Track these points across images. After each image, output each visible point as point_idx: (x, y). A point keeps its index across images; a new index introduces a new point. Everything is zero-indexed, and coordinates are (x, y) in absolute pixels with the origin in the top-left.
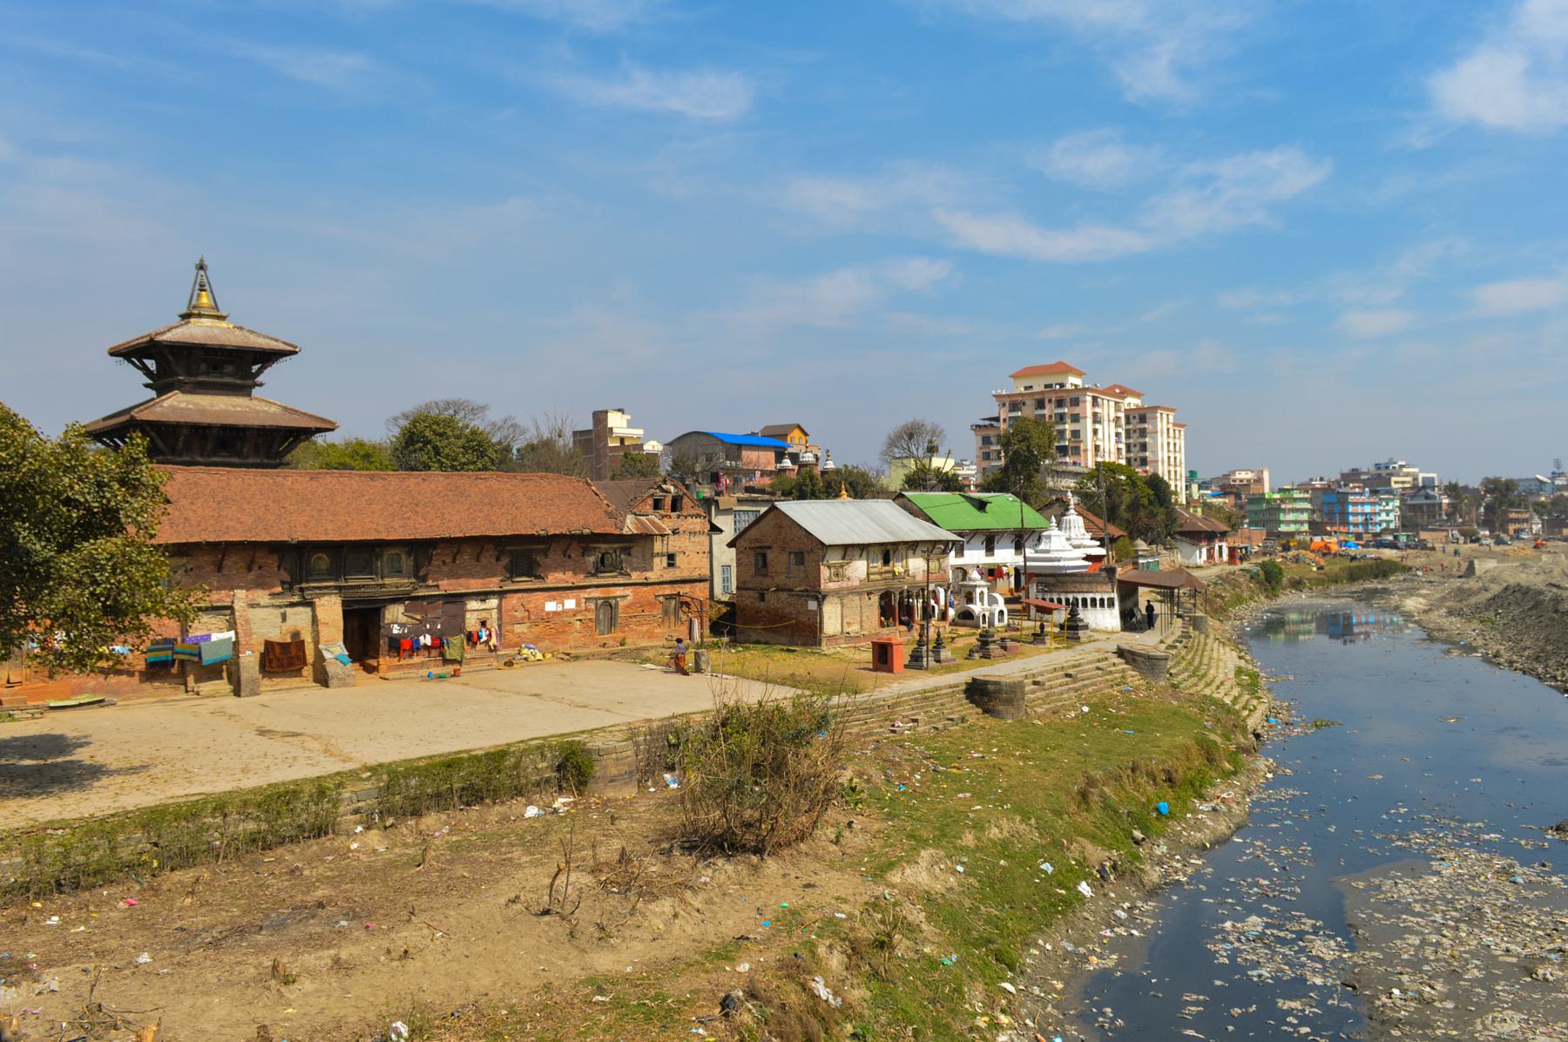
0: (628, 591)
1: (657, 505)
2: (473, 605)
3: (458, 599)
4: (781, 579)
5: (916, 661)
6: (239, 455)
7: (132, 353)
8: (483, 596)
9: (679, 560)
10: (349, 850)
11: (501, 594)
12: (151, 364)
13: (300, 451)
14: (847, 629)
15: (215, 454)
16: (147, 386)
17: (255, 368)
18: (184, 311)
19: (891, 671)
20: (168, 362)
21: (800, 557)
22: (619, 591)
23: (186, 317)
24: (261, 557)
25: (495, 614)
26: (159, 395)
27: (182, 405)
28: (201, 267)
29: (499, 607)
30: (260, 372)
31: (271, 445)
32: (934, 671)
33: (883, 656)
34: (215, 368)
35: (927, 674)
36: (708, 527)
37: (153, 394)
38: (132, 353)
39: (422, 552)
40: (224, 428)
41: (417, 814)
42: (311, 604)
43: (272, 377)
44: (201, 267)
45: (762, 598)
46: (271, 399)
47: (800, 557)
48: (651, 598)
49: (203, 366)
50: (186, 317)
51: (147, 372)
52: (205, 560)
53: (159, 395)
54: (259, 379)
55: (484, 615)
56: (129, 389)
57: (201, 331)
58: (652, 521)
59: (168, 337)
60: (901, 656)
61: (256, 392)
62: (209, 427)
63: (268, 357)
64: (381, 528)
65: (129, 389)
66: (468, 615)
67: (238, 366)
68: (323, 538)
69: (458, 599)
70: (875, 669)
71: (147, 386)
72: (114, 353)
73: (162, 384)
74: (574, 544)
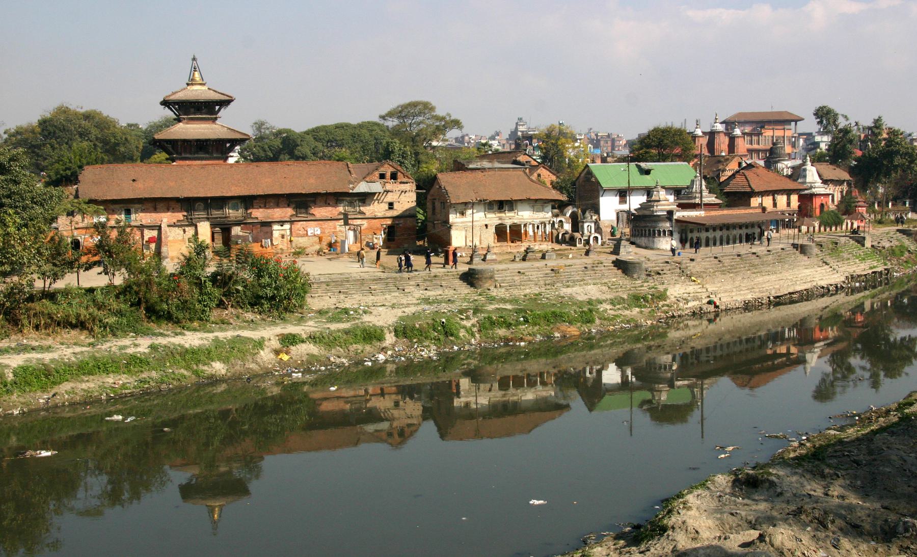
0: (365, 222)
1: (382, 176)
2: (276, 227)
3: (267, 224)
6: (207, 153)
7: (166, 103)
8: (282, 223)
9: (395, 206)
10: (303, 373)
11: (292, 222)
15: (197, 152)
24: (172, 204)
25: (288, 232)
28: (194, 59)
29: (291, 229)
30: (219, 110)
31: (217, 148)
38: (166, 103)
39: (248, 201)
40: (198, 141)
42: (196, 227)
43: (224, 113)
44: (194, 59)
46: (227, 123)
48: (379, 226)
52: (149, 205)
54: (219, 115)
55: (283, 232)
57: (198, 92)
58: (376, 187)
59: (171, 98)
61: (217, 122)
62: (207, 141)
63: (225, 103)
67: (207, 109)
68: (196, 196)
69: (267, 224)
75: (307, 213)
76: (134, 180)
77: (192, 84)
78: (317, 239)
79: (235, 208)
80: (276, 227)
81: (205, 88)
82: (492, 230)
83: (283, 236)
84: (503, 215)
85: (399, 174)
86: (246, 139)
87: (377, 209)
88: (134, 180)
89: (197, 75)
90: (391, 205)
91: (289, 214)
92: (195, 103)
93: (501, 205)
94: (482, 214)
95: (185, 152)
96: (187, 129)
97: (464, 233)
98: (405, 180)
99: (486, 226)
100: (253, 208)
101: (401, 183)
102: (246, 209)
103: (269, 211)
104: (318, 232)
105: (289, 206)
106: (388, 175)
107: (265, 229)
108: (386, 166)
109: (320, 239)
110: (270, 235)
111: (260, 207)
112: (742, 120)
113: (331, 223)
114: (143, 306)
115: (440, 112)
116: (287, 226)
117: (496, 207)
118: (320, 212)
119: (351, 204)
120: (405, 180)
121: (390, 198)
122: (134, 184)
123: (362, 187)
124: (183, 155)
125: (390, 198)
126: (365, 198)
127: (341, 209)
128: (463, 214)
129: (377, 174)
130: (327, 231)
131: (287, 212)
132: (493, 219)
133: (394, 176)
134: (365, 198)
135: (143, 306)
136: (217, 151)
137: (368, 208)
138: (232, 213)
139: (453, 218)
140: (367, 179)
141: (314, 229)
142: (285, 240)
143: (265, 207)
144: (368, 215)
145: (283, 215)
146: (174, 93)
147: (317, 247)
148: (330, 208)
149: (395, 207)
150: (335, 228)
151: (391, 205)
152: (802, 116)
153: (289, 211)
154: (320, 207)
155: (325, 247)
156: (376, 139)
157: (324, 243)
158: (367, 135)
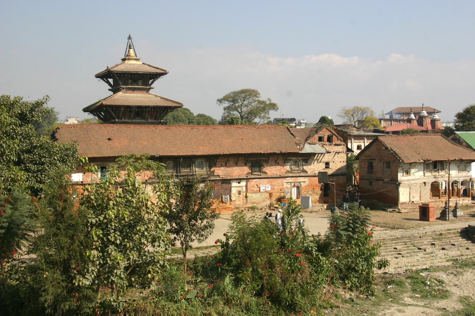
0: (306, 179)
1: (320, 139)
2: (234, 184)
3: (227, 182)
4: (379, 175)
5: (443, 216)
6: (144, 118)
7: (105, 76)
8: (239, 180)
11: (247, 179)
12: (111, 80)
13: (169, 116)
14: (412, 200)
15: (134, 118)
16: (109, 90)
17: (151, 81)
18: (123, 57)
19: (428, 220)
20: (118, 79)
21: (388, 165)
22: (301, 179)
23: (124, 60)
26: (114, 94)
27: (129, 97)
28: (130, 38)
29: (246, 186)
30: (153, 82)
32: (452, 222)
33: (424, 212)
34: (135, 82)
35: (448, 223)
36: (345, 150)
37: (111, 93)
38: (105, 76)
39: (212, 160)
41: (40, 183)
44: (130, 38)
45: (371, 183)
47: (388, 165)
49: (130, 81)
50: (124, 60)
51: (110, 84)
52: (396, 226)
53: (114, 94)
54: (152, 86)
55: (239, 189)
56: (101, 92)
57: (133, 66)
58: (317, 148)
59: (115, 69)
60: (435, 214)
61: (151, 91)
63: (155, 76)
64: (194, 150)
65: (101, 92)
66: (232, 189)
67: (144, 79)
69: (227, 182)
70: (421, 220)
71: (109, 90)
72: (97, 76)
73: (115, 89)
74: (280, 158)
75: (260, 171)
76: (109, 139)
77: (129, 59)
78: (267, 195)
79: (201, 166)
80: (234, 184)
81: (139, 63)
82: (429, 187)
83: (239, 193)
84: (437, 174)
85: (334, 137)
86: (176, 107)
87: (315, 168)
88: (109, 139)
89: (132, 51)
90: (327, 164)
91: (246, 172)
92: (134, 74)
93: (436, 165)
94: (421, 173)
95: (125, 118)
96: (127, 97)
97: (408, 189)
98: (338, 142)
99: (425, 183)
100: (215, 166)
101: (336, 145)
102: (210, 167)
103: (229, 169)
104: (269, 189)
105: (246, 164)
106: (326, 138)
107: (225, 186)
108: (324, 130)
109: (271, 195)
110: (229, 191)
111: (222, 166)
112: (402, 112)
113: (280, 181)
114: (267, 294)
115: (263, 98)
116: (243, 183)
117: (431, 167)
118: (271, 170)
119: (296, 163)
120: (338, 142)
121: (327, 158)
122: (110, 142)
123: (308, 149)
124: (123, 120)
125: (327, 158)
126: (308, 158)
127: (288, 168)
128: (408, 173)
129: (316, 136)
130: (276, 188)
131: (244, 170)
132: (430, 177)
133: (330, 139)
134: (308, 158)
135: (267, 294)
136: (151, 118)
137: (309, 167)
138: (199, 171)
139: (401, 177)
140: (309, 141)
141: (266, 186)
142: (241, 196)
143: (226, 165)
144: (309, 173)
145: (241, 173)
146: (117, 66)
147: (268, 202)
148: (279, 167)
149: (330, 166)
150: (283, 185)
151: (327, 164)
152: (437, 108)
153: (246, 170)
154: (271, 165)
155: (275, 202)
156: (189, 119)
157: (274, 199)
158: (183, 116)
